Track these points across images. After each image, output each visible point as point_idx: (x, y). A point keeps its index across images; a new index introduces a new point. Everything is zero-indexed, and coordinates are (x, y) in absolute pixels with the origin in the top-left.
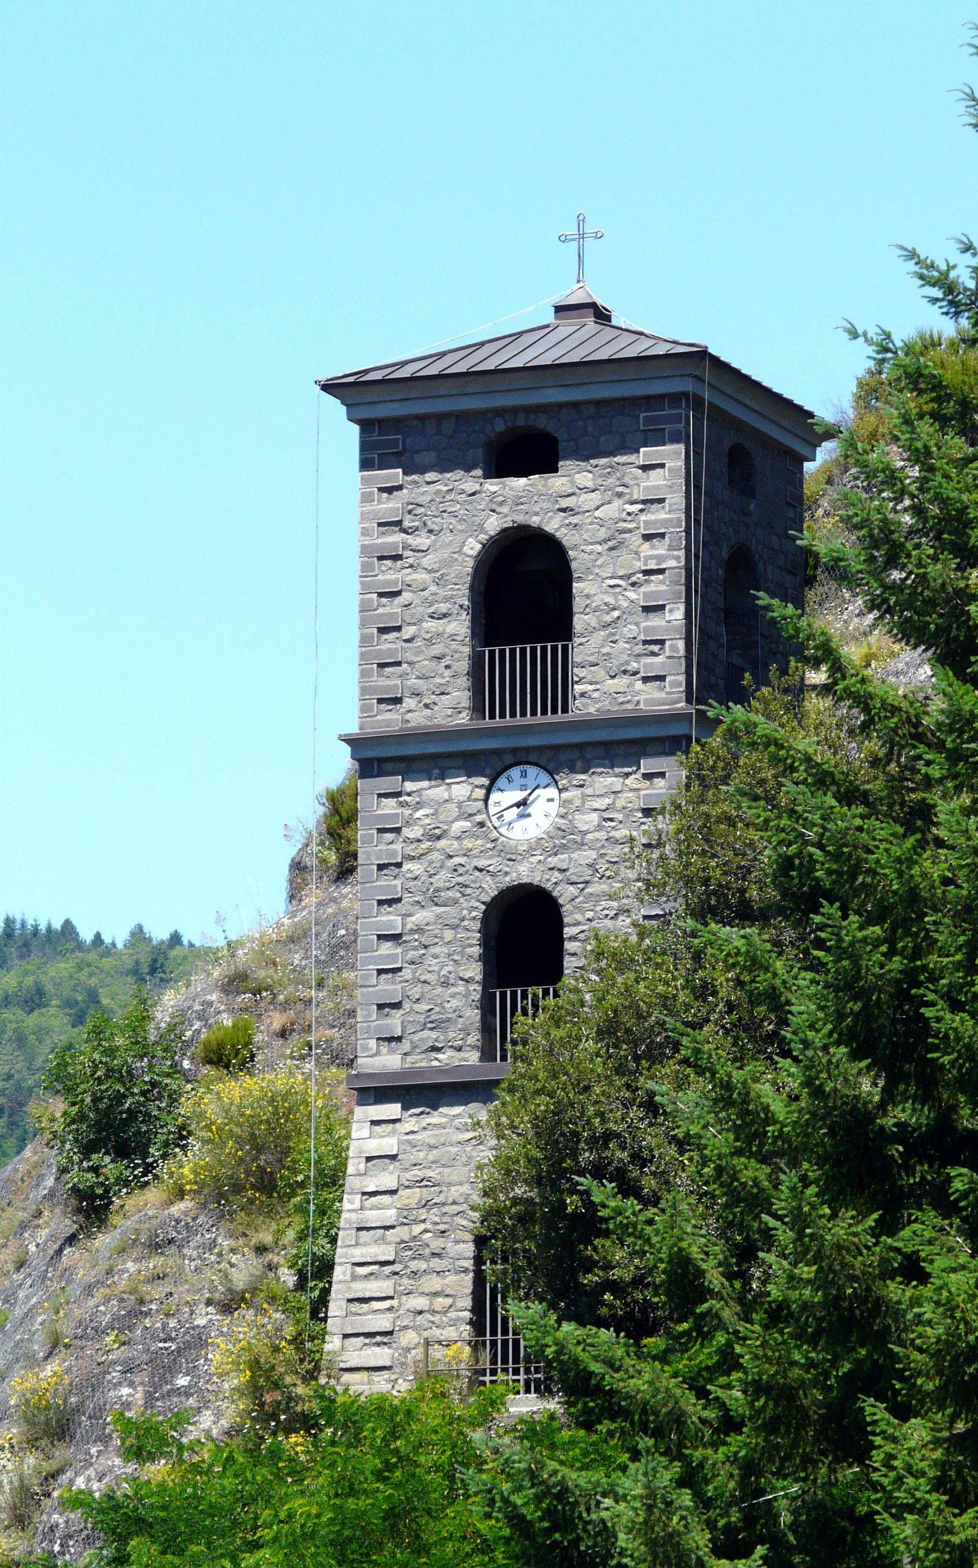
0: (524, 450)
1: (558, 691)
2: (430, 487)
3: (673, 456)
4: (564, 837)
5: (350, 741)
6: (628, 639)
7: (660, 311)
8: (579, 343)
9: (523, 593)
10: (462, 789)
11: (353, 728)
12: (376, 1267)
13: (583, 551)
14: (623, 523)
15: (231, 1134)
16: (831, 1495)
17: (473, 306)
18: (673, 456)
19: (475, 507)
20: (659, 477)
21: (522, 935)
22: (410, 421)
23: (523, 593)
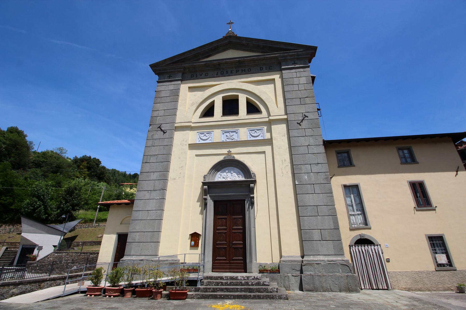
11: (203, 181)
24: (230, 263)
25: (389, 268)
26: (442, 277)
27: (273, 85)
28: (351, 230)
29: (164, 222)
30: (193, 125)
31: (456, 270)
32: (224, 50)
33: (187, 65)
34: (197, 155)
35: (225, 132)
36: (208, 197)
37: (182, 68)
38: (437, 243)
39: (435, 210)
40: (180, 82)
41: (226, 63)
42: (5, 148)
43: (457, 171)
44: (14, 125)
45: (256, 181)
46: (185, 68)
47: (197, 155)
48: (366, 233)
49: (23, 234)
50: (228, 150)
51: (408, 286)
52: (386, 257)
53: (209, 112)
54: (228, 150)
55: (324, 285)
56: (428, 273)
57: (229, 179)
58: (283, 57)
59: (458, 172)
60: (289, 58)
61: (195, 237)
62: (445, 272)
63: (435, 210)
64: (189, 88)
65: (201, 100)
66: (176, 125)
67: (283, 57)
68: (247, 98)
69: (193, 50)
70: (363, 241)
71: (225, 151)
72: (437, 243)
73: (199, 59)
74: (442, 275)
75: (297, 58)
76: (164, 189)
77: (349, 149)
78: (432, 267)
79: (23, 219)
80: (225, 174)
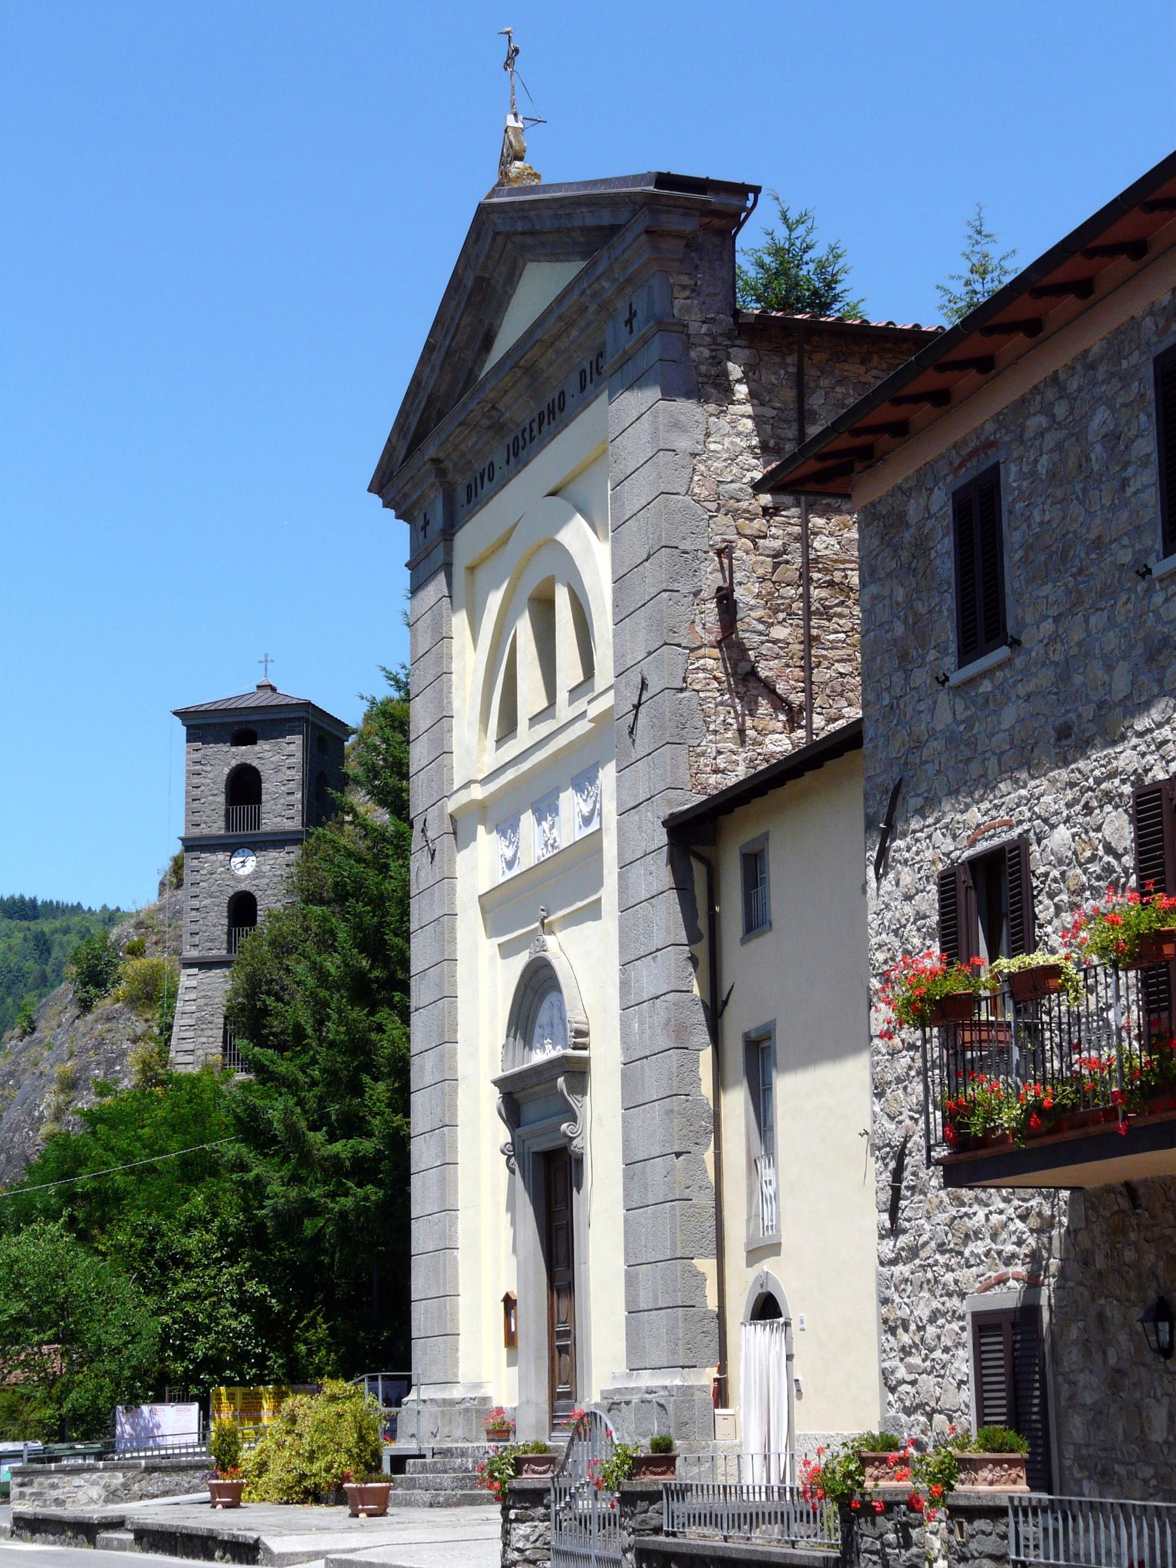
0: (245, 737)
1: (256, 822)
2: (212, 749)
3: (298, 739)
4: (257, 874)
6: (281, 805)
8: (265, 699)
9: (244, 787)
10: (221, 856)
12: (712, 1304)
13: (266, 773)
14: (280, 763)
17: (228, 684)
18: (298, 739)
19: (226, 757)
21: (242, 908)
22: (204, 726)
23: (244, 787)
69: (429, 348)
77: (763, 830)
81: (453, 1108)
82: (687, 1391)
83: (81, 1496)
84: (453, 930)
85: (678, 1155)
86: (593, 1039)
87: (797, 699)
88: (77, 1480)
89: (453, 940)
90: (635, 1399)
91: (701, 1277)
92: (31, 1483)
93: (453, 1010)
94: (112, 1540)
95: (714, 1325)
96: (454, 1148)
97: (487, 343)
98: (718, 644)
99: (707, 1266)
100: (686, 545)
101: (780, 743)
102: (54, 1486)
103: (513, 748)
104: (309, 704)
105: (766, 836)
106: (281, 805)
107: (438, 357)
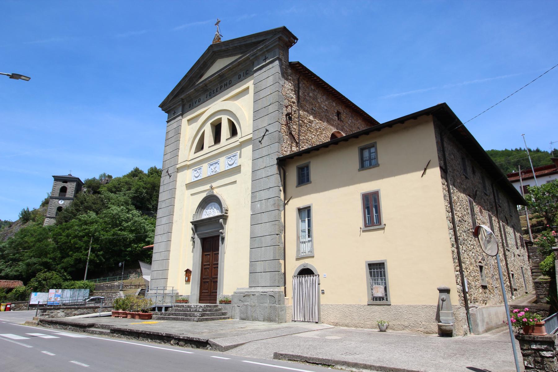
0: (65, 182)
1: (65, 196)
2: (59, 182)
3: (75, 183)
4: (64, 204)
5: (191, 222)
6: (70, 193)
7: (75, 175)
8: (70, 176)
9: (63, 190)
10: (57, 200)
11: (192, 221)
12: (283, 271)
13: (68, 188)
14: (71, 187)
15: (36, 216)
16: (97, 256)
17: (64, 173)
18: (75, 183)
19: (61, 184)
20: (74, 184)
21: (60, 209)
22: (57, 179)
23: (63, 190)
24: (210, 295)
25: (324, 300)
26: (374, 312)
27: (57, 195)
28: (297, 259)
29: (170, 261)
30: (188, 163)
31: (390, 305)
32: (212, 63)
33: (182, 96)
34: (192, 195)
35: (211, 165)
36: (196, 236)
37: (179, 102)
38: (377, 270)
39: (383, 229)
40: (180, 117)
41: (211, 82)
42: (147, 193)
43: (425, 169)
44: (153, 166)
45: (227, 216)
46: (182, 99)
47: (192, 195)
48: (309, 263)
49: (144, 277)
50: (210, 185)
51: (336, 321)
52: (321, 288)
53: (200, 146)
54: (210, 185)
55: (254, 315)
56: (359, 307)
57: (211, 216)
58: (253, 55)
59: (427, 171)
60: (259, 53)
61: (188, 272)
62: (377, 307)
63: (383, 229)
64: (188, 121)
65: (195, 133)
66: (178, 166)
67: (253, 55)
68: (229, 119)
69: (186, 76)
70: (306, 272)
71: (207, 187)
72: (377, 270)
73: (195, 83)
74: (373, 310)
75: (267, 51)
76: (170, 232)
77: (373, 141)
78: (365, 299)
79: (141, 264)
80: (209, 210)
81: (171, 229)
82: (279, 292)
83: (59, 315)
84: (175, 192)
85: (277, 235)
86: (229, 212)
87: (298, 141)
88: (58, 311)
89: (175, 194)
90: (257, 294)
91: (280, 264)
92: (45, 312)
93: (173, 208)
94: (96, 331)
95: (283, 276)
96: (171, 237)
97: (201, 77)
98: (286, 125)
99: (282, 262)
100: (281, 103)
101: (295, 149)
102: (52, 313)
103: (217, 146)
104: (298, 63)
105: (310, 162)
106: (70, 193)
107: (187, 79)
